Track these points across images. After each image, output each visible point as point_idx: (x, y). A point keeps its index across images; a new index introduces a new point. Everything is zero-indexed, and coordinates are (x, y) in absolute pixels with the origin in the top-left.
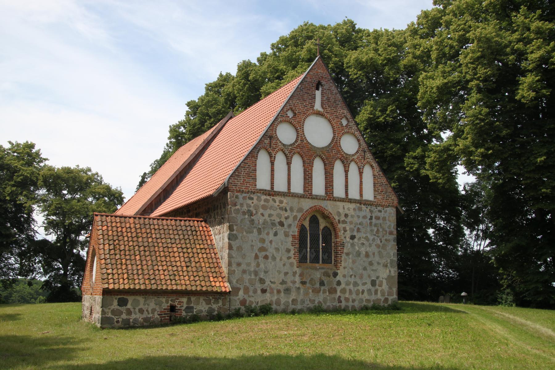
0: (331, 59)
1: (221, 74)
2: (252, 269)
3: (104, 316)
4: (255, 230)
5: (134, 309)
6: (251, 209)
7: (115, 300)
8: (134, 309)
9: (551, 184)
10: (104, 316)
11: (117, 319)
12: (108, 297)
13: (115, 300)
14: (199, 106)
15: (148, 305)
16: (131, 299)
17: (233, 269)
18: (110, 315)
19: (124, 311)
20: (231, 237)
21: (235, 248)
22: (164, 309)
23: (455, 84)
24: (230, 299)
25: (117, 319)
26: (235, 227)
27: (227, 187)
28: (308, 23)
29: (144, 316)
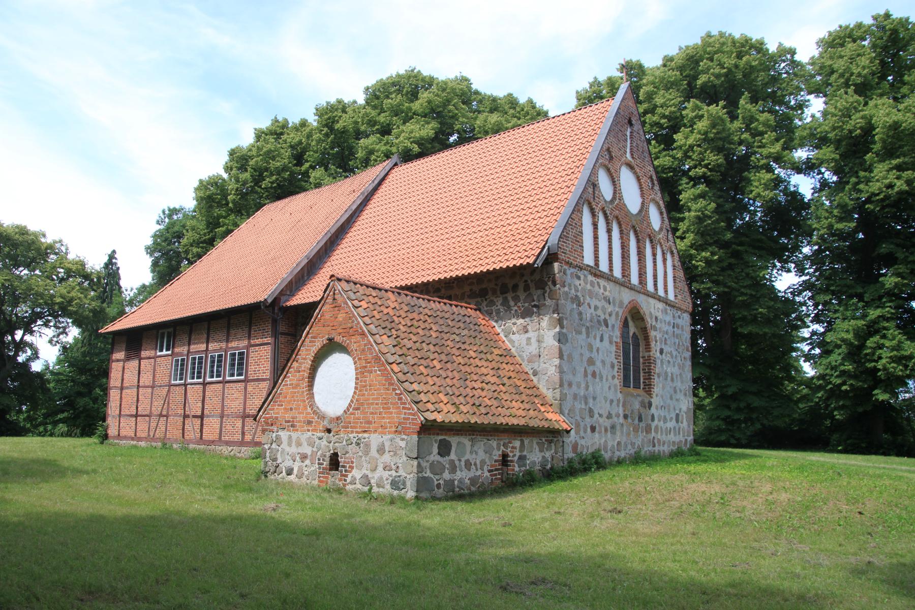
0: (457, 120)
1: (276, 118)
2: (582, 394)
3: (420, 475)
4: (584, 330)
5: (460, 460)
6: (579, 294)
7: (434, 443)
8: (460, 460)
9: (767, 304)
10: (420, 475)
11: (437, 480)
12: (425, 438)
13: (434, 443)
14: (251, 157)
15: (476, 453)
16: (454, 440)
17: (565, 392)
18: (428, 474)
19: (447, 466)
20: (561, 339)
21: (565, 357)
22: (496, 461)
23: (666, 169)
24: (563, 442)
25: (437, 480)
26: (565, 322)
27: (556, 254)
28: (415, 68)
29: (471, 474)
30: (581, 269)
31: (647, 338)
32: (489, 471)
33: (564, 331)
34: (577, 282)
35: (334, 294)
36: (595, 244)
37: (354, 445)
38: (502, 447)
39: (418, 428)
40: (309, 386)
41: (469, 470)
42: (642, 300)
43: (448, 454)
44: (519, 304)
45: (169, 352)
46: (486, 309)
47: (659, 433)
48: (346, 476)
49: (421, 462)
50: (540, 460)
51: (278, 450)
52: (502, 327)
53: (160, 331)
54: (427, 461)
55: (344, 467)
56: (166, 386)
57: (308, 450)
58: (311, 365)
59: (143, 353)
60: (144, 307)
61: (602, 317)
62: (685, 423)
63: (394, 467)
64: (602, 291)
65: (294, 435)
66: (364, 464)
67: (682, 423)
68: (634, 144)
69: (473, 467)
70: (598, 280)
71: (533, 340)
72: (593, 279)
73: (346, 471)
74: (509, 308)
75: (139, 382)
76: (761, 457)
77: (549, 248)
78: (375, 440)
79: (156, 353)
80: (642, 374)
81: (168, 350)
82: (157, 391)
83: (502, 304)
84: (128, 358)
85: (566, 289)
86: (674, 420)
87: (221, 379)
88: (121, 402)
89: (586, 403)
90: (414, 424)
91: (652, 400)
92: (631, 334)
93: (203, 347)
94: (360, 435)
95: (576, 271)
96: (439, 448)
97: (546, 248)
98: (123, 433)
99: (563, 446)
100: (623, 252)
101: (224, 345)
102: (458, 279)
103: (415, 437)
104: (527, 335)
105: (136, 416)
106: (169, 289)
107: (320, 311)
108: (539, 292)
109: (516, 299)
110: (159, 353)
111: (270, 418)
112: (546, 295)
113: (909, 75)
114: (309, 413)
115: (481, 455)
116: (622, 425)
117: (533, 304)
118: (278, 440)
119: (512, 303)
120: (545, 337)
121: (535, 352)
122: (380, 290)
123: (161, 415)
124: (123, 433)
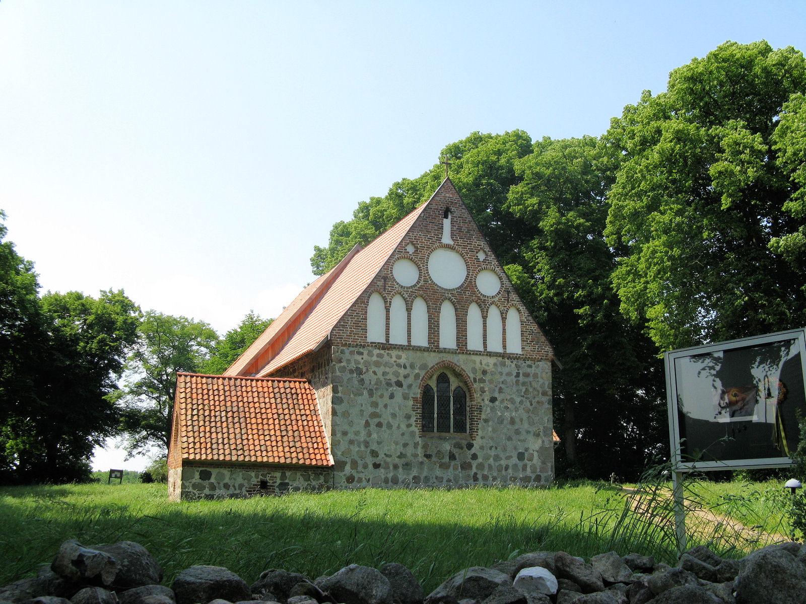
8: (219, 483)
26: (340, 389)
43: (209, 479)
69: (231, 487)
102: (342, 319)
113: (804, 189)
115: (240, 480)
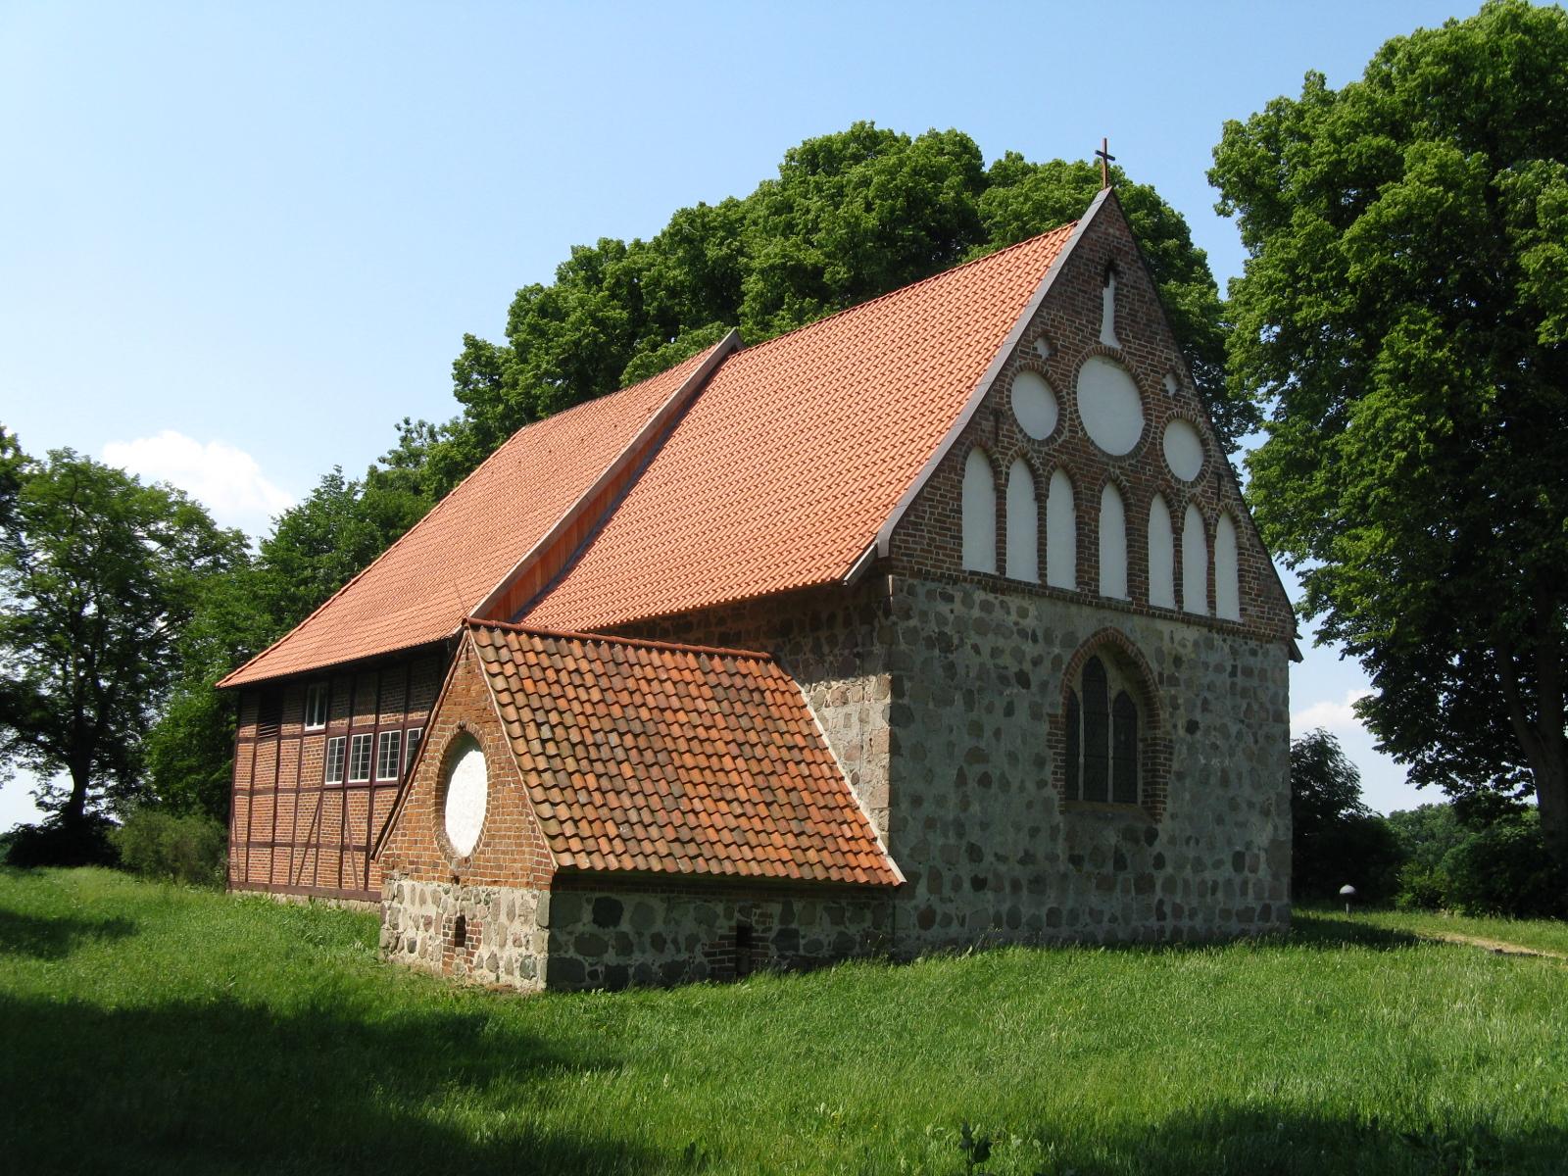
2: (951, 817)
4: (958, 697)
5: (640, 934)
6: (948, 630)
7: (585, 904)
10: (555, 955)
11: (591, 965)
15: (678, 923)
16: (629, 902)
18: (572, 953)
19: (612, 942)
22: (722, 937)
25: (591, 965)
26: (907, 685)
30: (955, 581)
31: (1150, 703)
32: (707, 955)
33: (905, 701)
34: (943, 608)
35: (467, 650)
36: (998, 529)
37: (482, 903)
38: (737, 915)
39: (549, 878)
40: (436, 804)
41: (662, 951)
42: (1133, 628)
43: (616, 922)
44: (836, 651)
45: (322, 727)
46: (789, 658)
47: (418, 891)
48: (472, 955)
49: (557, 933)
50: (833, 938)
51: (400, 911)
52: (812, 693)
53: (310, 687)
54: (570, 933)
55: (471, 939)
56: (316, 789)
57: (431, 911)
58: (440, 770)
59: (283, 727)
60: (295, 638)
61: (1014, 669)
62: (1263, 872)
63: (524, 941)
64: (1014, 617)
65: (419, 885)
66: (493, 935)
67: (1254, 870)
68: (1125, 312)
69: (670, 945)
70: (1001, 597)
71: (855, 719)
72: (991, 597)
73: (473, 947)
74: (821, 660)
75: (277, 782)
76: (1409, 940)
77: (876, 545)
78: (505, 894)
79: (303, 728)
80: (1140, 774)
81: (320, 723)
82: (304, 797)
83: (812, 651)
84: (259, 738)
85: (913, 623)
86: (1228, 866)
87: (367, 780)
88: (250, 817)
89: (960, 835)
90: (546, 872)
91: (1159, 827)
92: (1112, 694)
93: (370, 719)
94: (490, 888)
95: (942, 585)
96: (594, 911)
97: (872, 547)
98: (253, 878)
99: (893, 915)
100: (1078, 535)
101: (401, 717)
103: (547, 894)
104: (847, 709)
105: (272, 845)
106: (338, 602)
107: (451, 679)
108: (865, 629)
109: (832, 641)
110: (308, 729)
111: (392, 855)
112: (875, 634)
114: (434, 850)
115: (689, 925)
116: (1065, 876)
117: (855, 651)
118: (397, 896)
119: (826, 649)
120: (871, 713)
121: (856, 741)
122: (557, 638)
123: (307, 845)
124: (253, 878)
